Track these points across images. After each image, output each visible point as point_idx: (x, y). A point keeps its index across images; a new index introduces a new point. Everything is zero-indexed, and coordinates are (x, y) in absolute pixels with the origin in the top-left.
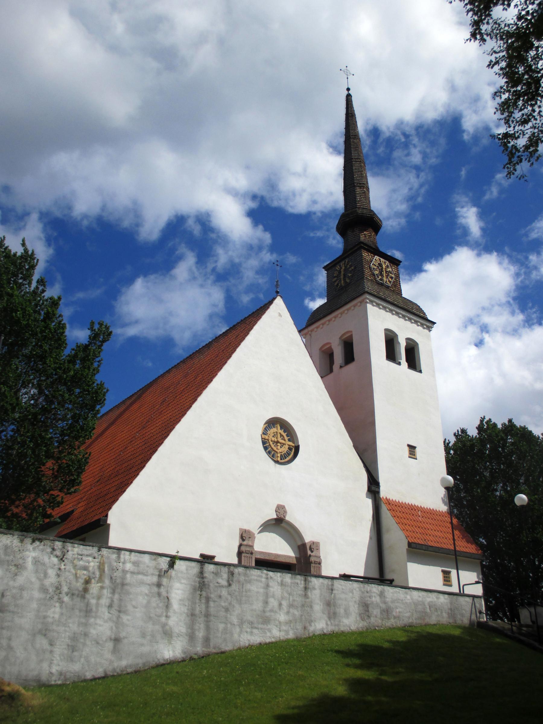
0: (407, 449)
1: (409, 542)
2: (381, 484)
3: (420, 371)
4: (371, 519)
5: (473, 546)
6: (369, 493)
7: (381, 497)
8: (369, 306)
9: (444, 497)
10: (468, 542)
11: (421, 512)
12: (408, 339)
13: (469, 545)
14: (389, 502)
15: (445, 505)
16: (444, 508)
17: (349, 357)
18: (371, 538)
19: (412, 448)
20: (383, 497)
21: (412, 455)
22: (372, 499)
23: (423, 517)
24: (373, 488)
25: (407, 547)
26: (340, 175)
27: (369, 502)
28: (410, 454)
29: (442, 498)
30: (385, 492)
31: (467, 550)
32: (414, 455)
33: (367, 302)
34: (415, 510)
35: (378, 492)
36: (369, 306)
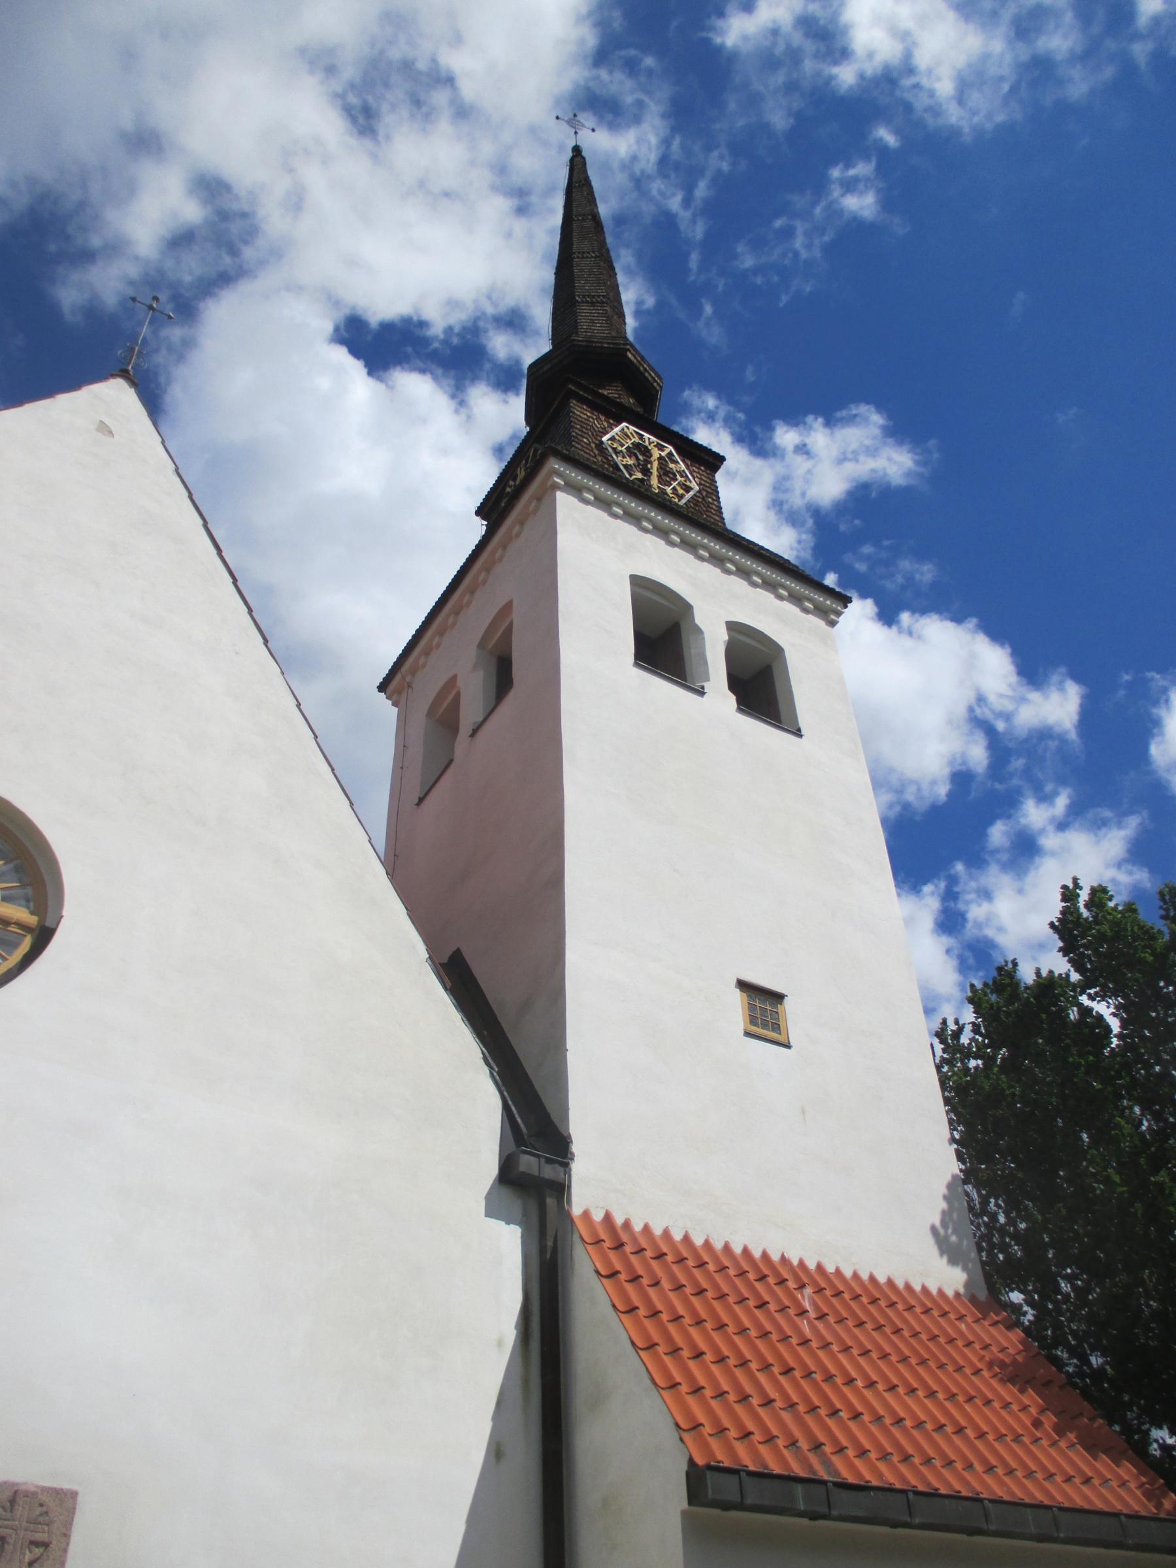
0: (737, 999)
1: (691, 1462)
2: (575, 1148)
3: (798, 733)
4: (509, 1333)
5: (1127, 1471)
6: (506, 1193)
7: (576, 1210)
8: (565, 502)
9: (944, 1223)
10: (1092, 1446)
11: (820, 1291)
12: (734, 627)
13: (1103, 1464)
14: (614, 1236)
15: (953, 1261)
16: (950, 1279)
17: (503, 677)
18: (496, 1452)
19: (763, 1005)
20: (586, 1215)
21: (765, 1025)
22: (524, 1224)
23: (822, 1317)
24: (528, 1163)
25: (685, 1504)
26: (544, 290)
27: (506, 1243)
28: (753, 1020)
29: (933, 1229)
30: (598, 1184)
31: (1076, 1496)
32: (776, 1027)
33: (556, 487)
34: (782, 1282)
35: (561, 1189)
36: (565, 502)
